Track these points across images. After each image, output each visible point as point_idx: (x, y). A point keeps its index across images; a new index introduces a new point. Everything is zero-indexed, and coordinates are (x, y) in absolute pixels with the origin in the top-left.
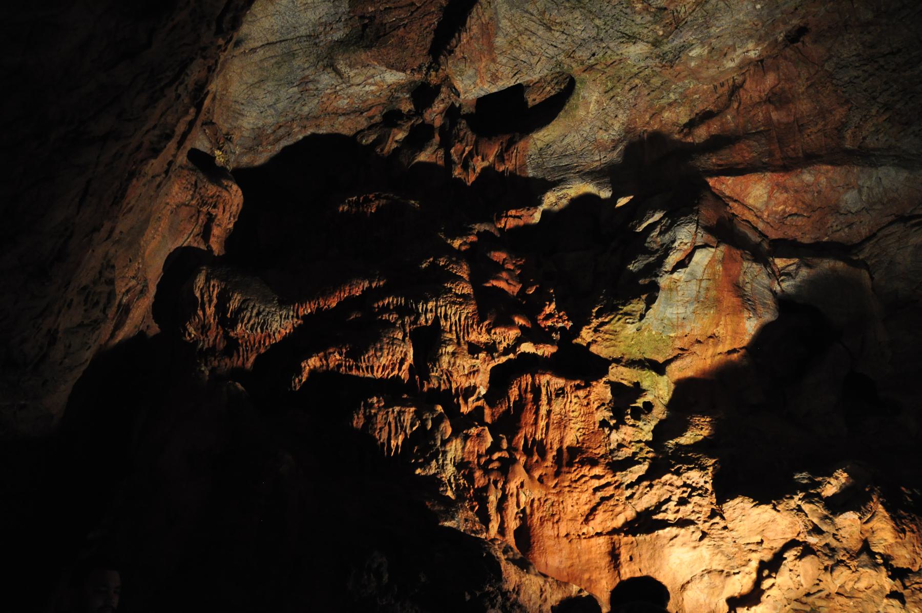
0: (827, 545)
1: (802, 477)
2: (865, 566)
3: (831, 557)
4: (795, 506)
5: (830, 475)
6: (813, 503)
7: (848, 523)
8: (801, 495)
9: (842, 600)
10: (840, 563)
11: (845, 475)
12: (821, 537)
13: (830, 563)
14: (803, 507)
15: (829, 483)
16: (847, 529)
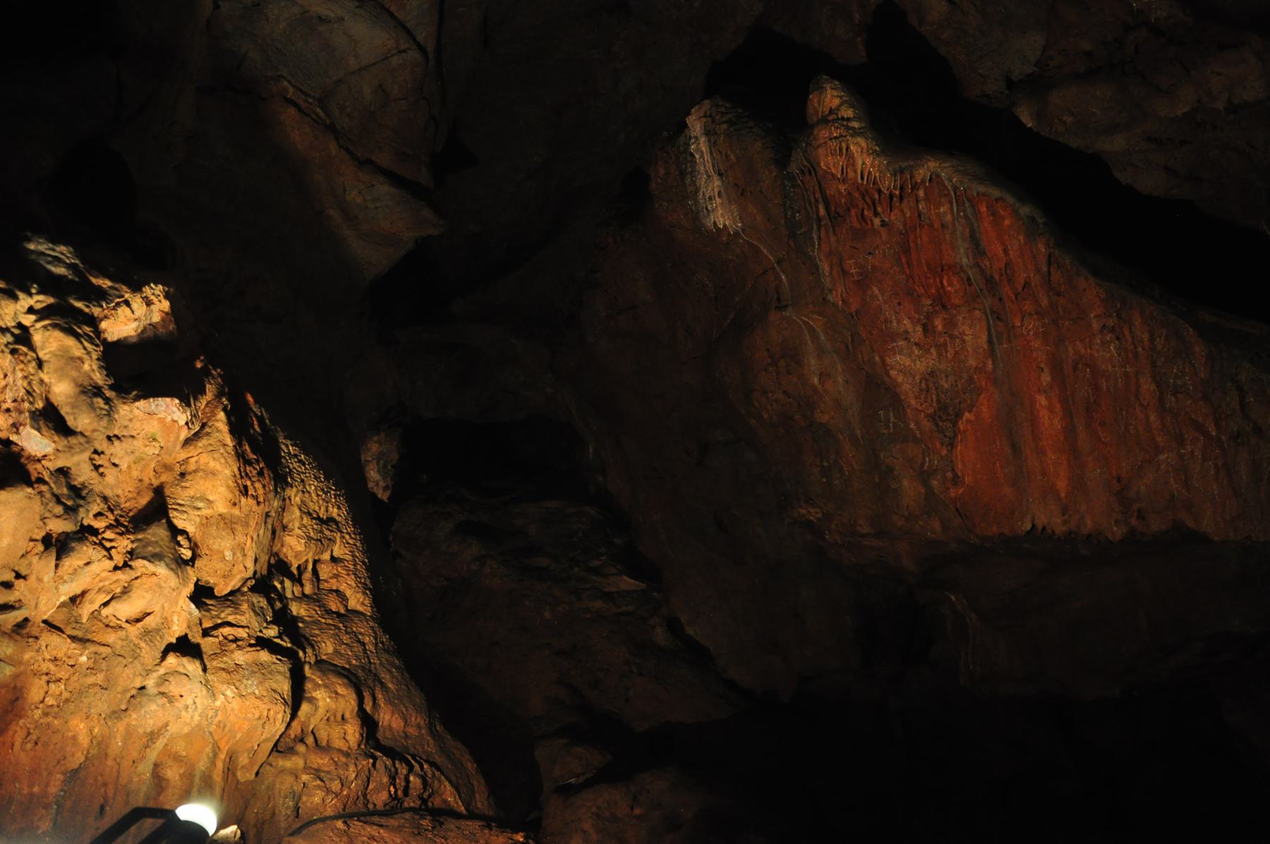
0: (63, 472)
1: (58, 257)
2: (154, 558)
3: (71, 511)
4: (11, 324)
5: (137, 288)
6: (77, 336)
7: (153, 427)
8: (40, 300)
9: (57, 644)
10: (86, 532)
11: (166, 305)
12: (62, 442)
13: (59, 526)
14: (37, 338)
15: (127, 303)
16: (137, 443)
